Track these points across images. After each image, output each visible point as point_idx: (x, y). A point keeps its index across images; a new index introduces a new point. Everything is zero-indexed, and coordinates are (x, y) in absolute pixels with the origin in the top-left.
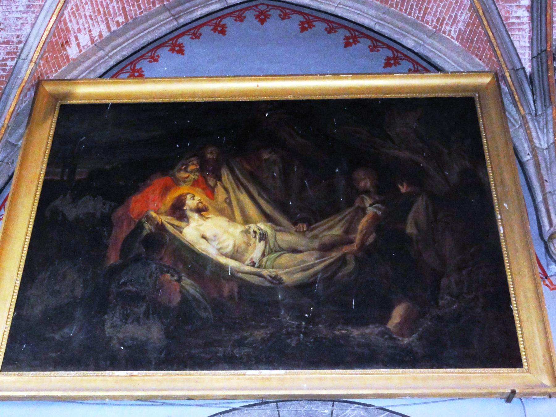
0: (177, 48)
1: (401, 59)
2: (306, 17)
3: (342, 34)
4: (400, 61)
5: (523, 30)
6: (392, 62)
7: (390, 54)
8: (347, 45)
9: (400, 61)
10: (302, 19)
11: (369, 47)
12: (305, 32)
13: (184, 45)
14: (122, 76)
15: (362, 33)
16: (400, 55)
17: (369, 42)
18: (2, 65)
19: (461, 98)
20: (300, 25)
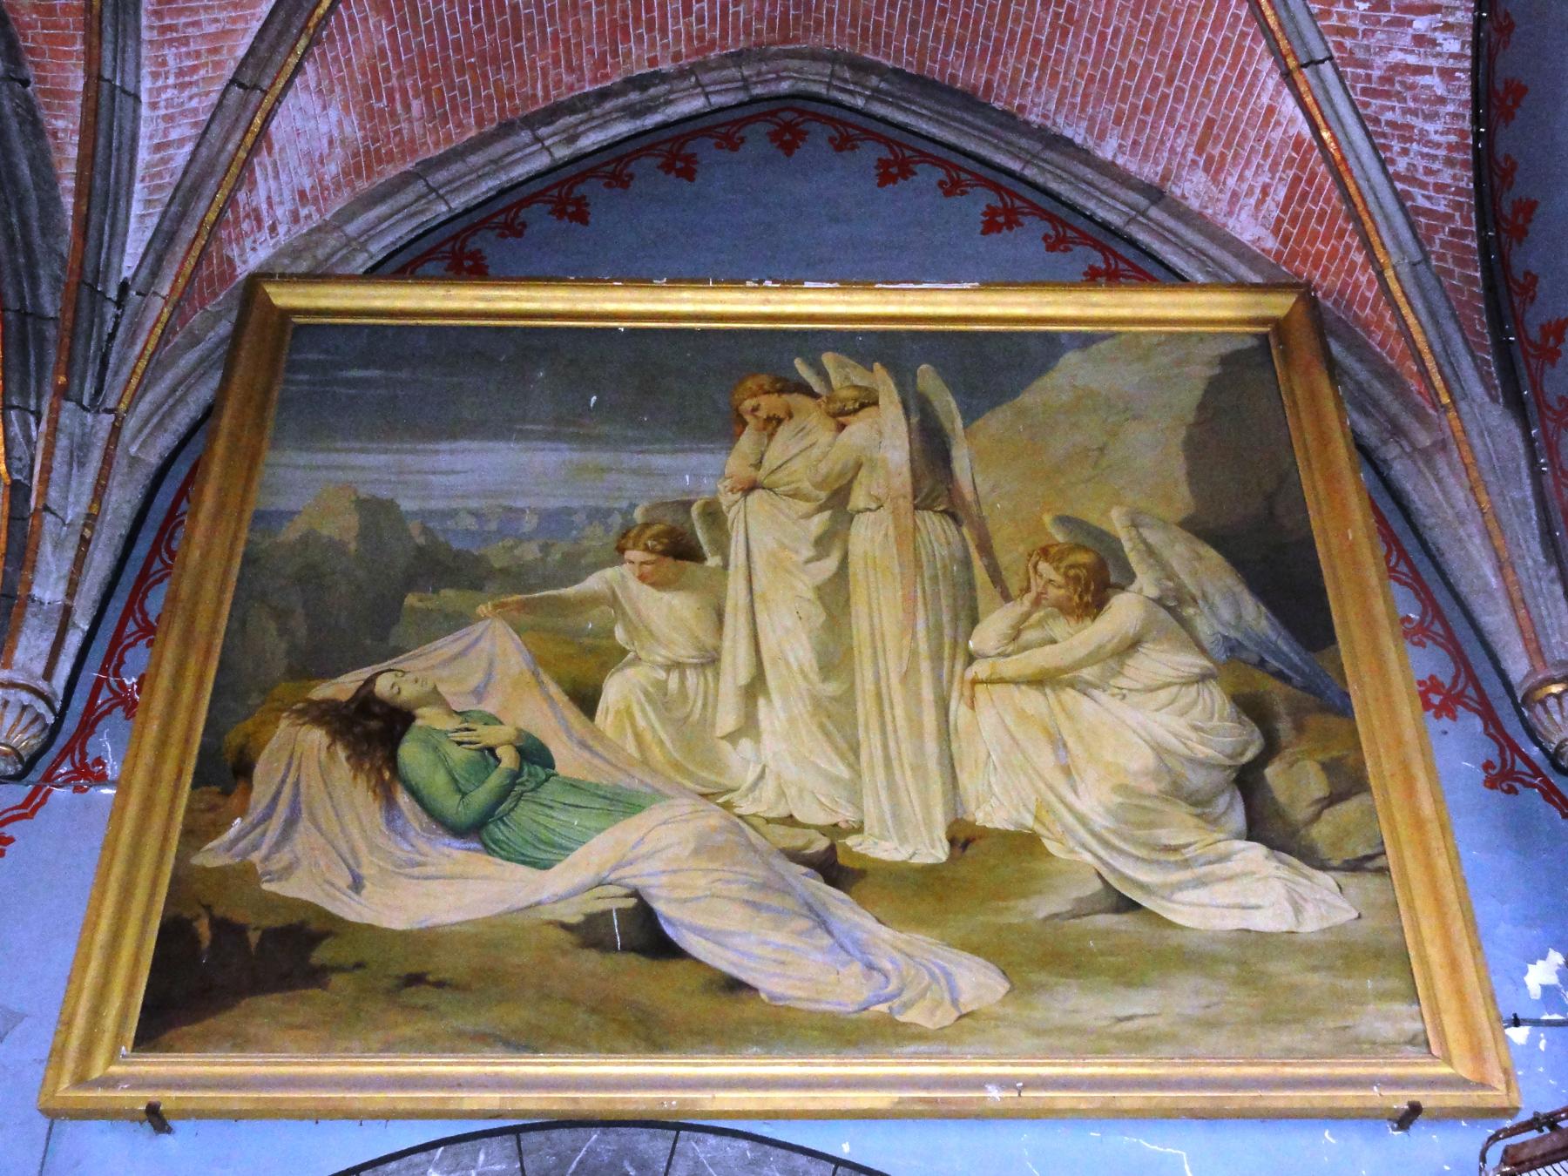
0: (679, 165)
1: (1023, 214)
2: (1112, 262)
3: (979, 201)
4: (1021, 219)
5: (736, 40)
6: (1001, 219)
7: (992, 199)
8: (990, 227)
9: (1021, 219)
10: (885, 153)
11: (941, 184)
12: (994, 236)
13: (698, 158)
14: (430, 268)
15: (865, 131)
16: (851, 131)
17: (940, 174)
18: (575, 4)
19: (437, 638)
20: (984, 214)
